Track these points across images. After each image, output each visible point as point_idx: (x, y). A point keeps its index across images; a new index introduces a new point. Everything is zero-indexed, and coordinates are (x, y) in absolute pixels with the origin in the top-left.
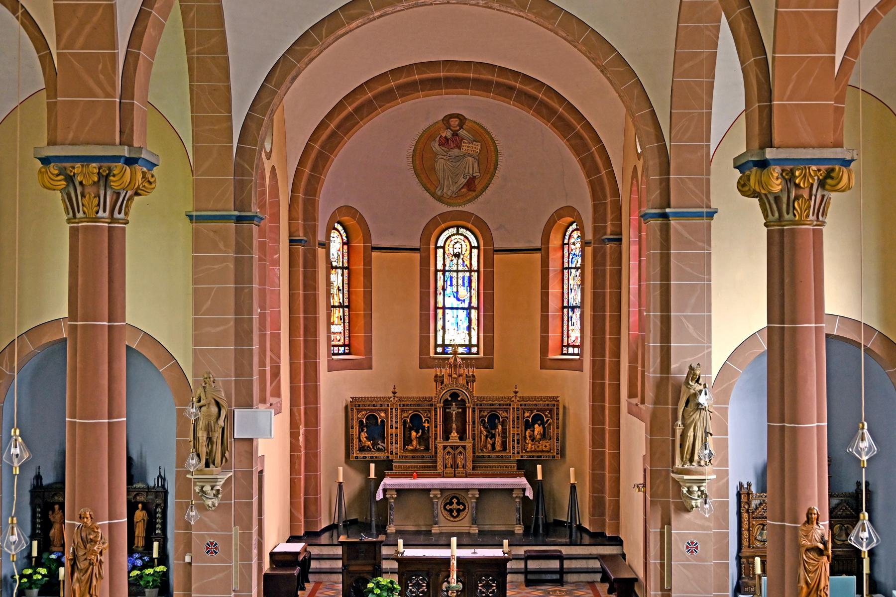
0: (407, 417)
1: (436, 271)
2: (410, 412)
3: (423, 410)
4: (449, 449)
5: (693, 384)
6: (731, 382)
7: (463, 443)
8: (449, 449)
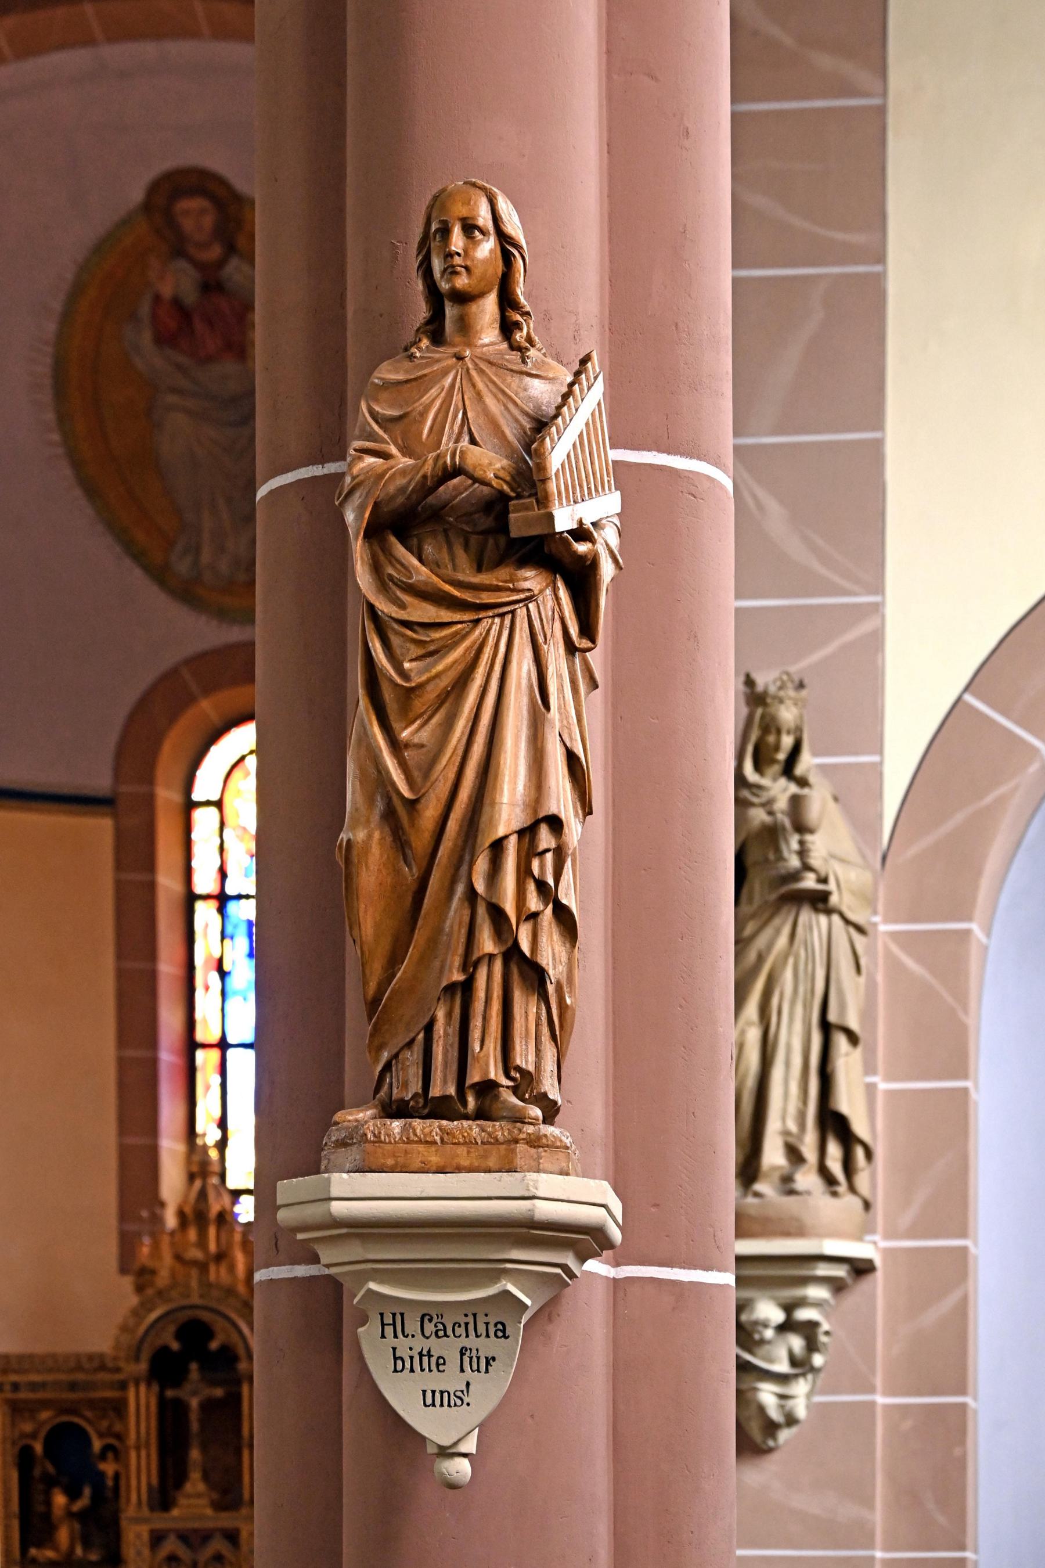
0: (34, 1436)
1: (191, 898)
2: (45, 1415)
3: (92, 1404)
4: (171, 1545)
5: (765, 782)
6: (989, 799)
7: (226, 1520)
8: (171, 1545)
